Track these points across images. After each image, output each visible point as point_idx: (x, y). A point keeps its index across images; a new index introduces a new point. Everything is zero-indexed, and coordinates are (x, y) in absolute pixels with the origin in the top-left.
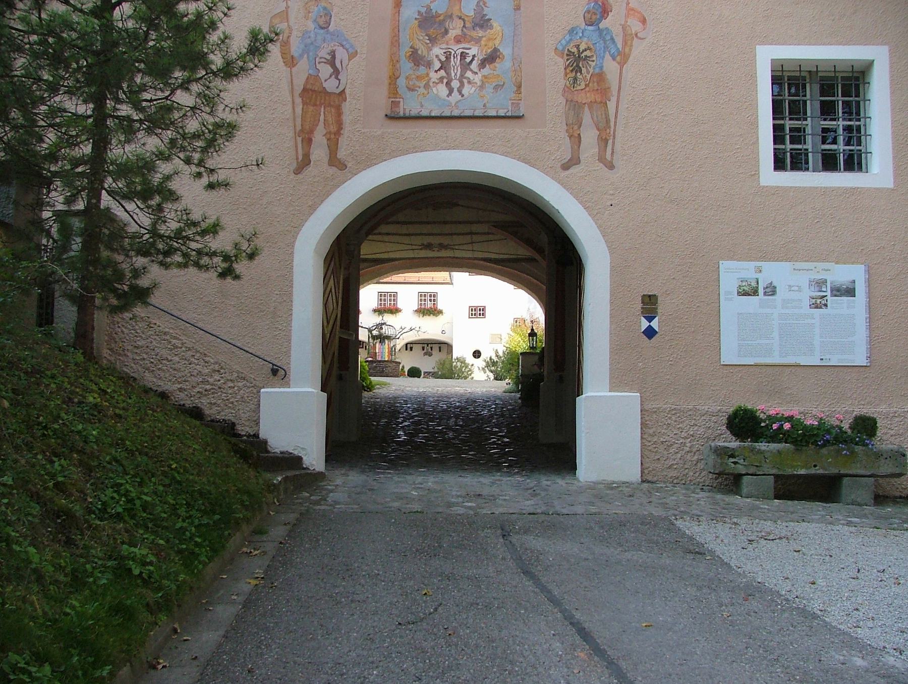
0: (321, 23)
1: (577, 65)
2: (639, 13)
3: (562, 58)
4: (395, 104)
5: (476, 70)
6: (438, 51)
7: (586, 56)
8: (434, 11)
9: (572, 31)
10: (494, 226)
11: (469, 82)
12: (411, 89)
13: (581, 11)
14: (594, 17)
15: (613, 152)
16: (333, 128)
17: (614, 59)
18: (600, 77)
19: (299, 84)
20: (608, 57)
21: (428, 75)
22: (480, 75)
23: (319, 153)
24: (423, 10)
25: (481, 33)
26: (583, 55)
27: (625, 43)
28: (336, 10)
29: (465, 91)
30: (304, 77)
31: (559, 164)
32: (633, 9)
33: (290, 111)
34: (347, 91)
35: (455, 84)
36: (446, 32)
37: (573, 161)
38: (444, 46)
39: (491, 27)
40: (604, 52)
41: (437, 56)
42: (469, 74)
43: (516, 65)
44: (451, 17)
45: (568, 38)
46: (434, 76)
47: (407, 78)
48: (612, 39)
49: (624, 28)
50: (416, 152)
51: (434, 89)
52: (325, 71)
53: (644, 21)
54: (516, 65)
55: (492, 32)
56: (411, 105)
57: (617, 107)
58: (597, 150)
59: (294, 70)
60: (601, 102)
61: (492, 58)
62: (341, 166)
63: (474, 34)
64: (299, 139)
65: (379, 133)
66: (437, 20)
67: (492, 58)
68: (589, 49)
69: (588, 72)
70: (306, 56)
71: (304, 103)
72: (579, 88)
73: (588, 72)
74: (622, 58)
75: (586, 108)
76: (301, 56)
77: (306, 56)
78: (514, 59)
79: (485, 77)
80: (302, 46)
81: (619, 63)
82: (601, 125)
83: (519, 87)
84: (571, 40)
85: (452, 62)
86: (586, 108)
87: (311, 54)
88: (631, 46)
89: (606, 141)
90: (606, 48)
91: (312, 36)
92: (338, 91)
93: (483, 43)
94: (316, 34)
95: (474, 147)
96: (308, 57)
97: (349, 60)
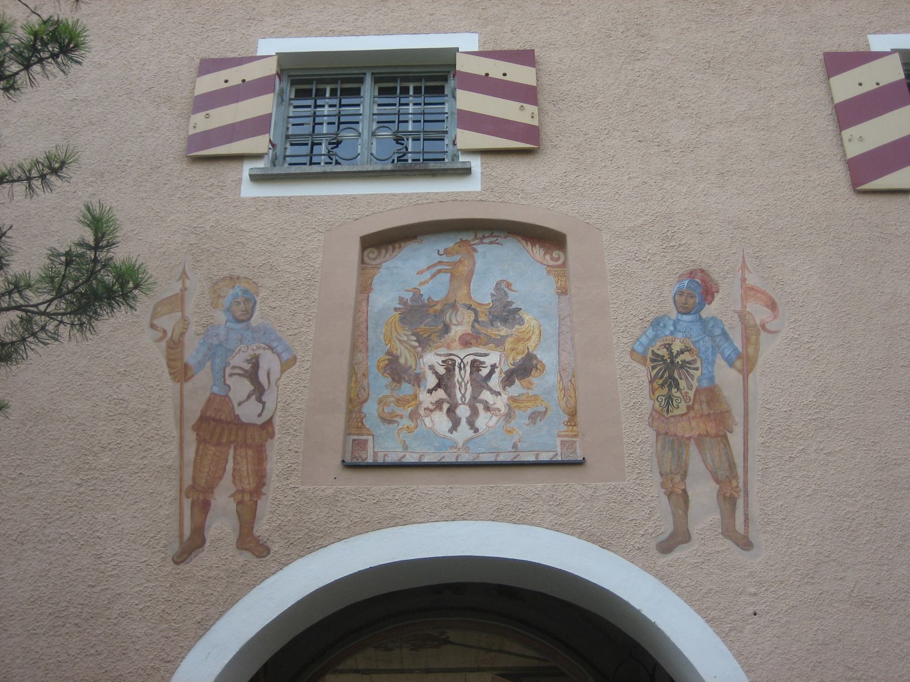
0: (238, 313)
1: (671, 376)
2: (764, 293)
3: (644, 364)
4: (360, 445)
6: (432, 359)
7: (684, 361)
8: (425, 297)
9: (657, 323)
10: (501, 675)
11: (487, 408)
12: (388, 420)
13: (669, 292)
14: (691, 301)
15: (747, 519)
16: (249, 484)
17: (731, 365)
18: (711, 394)
19: (195, 408)
20: (720, 361)
21: (415, 397)
22: (504, 397)
23: (222, 526)
24: (408, 296)
25: (504, 331)
26: (679, 359)
27: (746, 340)
28: (263, 293)
30: (203, 397)
31: (653, 544)
32: (752, 289)
33: (175, 453)
34: (277, 421)
35: (463, 412)
36: (447, 329)
37: (678, 538)
38: (443, 351)
39: (521, 322)
40: (714, 354)
41: (431, 367)
42: (486, 395)
43: (566, 380)
44: (454, 306)
45: (650, 333)
47: (380, 402)
48: (724, 334)
49: (742, 316)
50: (396, 525)
51: (427, 421)
52: (241, 388)
54: (566, 380)
55: (523, 328)
56: (386, 445)
57: (746, 443)
58: (718, 516)
59: (188, 386)
61: (525, 369)
62: (260, 550)
64: (187, 503)
65: (329, 492)
66: (431, 311)
67: (525, 369)
69: (690, 387)
70: (208, 364)
71: (200, 440)
72: (677, 412)
73: (690, 387)
74: (745, 363)
75: (693, 447)
76: (201, 365)
77: (208, 364)
78: (561, 371)
79: (513, 399)
81: (740, 371)
83: (573, 414)
84: (656, 337)
87: (218, 360)
88: (757, 343)
89: (732, 501)
90: (716, 349)
91: (222, 332)
92: (260, 421)
93: (508, 345)
95: (498, 515)
96: (213, 370)
97: (283, 371)
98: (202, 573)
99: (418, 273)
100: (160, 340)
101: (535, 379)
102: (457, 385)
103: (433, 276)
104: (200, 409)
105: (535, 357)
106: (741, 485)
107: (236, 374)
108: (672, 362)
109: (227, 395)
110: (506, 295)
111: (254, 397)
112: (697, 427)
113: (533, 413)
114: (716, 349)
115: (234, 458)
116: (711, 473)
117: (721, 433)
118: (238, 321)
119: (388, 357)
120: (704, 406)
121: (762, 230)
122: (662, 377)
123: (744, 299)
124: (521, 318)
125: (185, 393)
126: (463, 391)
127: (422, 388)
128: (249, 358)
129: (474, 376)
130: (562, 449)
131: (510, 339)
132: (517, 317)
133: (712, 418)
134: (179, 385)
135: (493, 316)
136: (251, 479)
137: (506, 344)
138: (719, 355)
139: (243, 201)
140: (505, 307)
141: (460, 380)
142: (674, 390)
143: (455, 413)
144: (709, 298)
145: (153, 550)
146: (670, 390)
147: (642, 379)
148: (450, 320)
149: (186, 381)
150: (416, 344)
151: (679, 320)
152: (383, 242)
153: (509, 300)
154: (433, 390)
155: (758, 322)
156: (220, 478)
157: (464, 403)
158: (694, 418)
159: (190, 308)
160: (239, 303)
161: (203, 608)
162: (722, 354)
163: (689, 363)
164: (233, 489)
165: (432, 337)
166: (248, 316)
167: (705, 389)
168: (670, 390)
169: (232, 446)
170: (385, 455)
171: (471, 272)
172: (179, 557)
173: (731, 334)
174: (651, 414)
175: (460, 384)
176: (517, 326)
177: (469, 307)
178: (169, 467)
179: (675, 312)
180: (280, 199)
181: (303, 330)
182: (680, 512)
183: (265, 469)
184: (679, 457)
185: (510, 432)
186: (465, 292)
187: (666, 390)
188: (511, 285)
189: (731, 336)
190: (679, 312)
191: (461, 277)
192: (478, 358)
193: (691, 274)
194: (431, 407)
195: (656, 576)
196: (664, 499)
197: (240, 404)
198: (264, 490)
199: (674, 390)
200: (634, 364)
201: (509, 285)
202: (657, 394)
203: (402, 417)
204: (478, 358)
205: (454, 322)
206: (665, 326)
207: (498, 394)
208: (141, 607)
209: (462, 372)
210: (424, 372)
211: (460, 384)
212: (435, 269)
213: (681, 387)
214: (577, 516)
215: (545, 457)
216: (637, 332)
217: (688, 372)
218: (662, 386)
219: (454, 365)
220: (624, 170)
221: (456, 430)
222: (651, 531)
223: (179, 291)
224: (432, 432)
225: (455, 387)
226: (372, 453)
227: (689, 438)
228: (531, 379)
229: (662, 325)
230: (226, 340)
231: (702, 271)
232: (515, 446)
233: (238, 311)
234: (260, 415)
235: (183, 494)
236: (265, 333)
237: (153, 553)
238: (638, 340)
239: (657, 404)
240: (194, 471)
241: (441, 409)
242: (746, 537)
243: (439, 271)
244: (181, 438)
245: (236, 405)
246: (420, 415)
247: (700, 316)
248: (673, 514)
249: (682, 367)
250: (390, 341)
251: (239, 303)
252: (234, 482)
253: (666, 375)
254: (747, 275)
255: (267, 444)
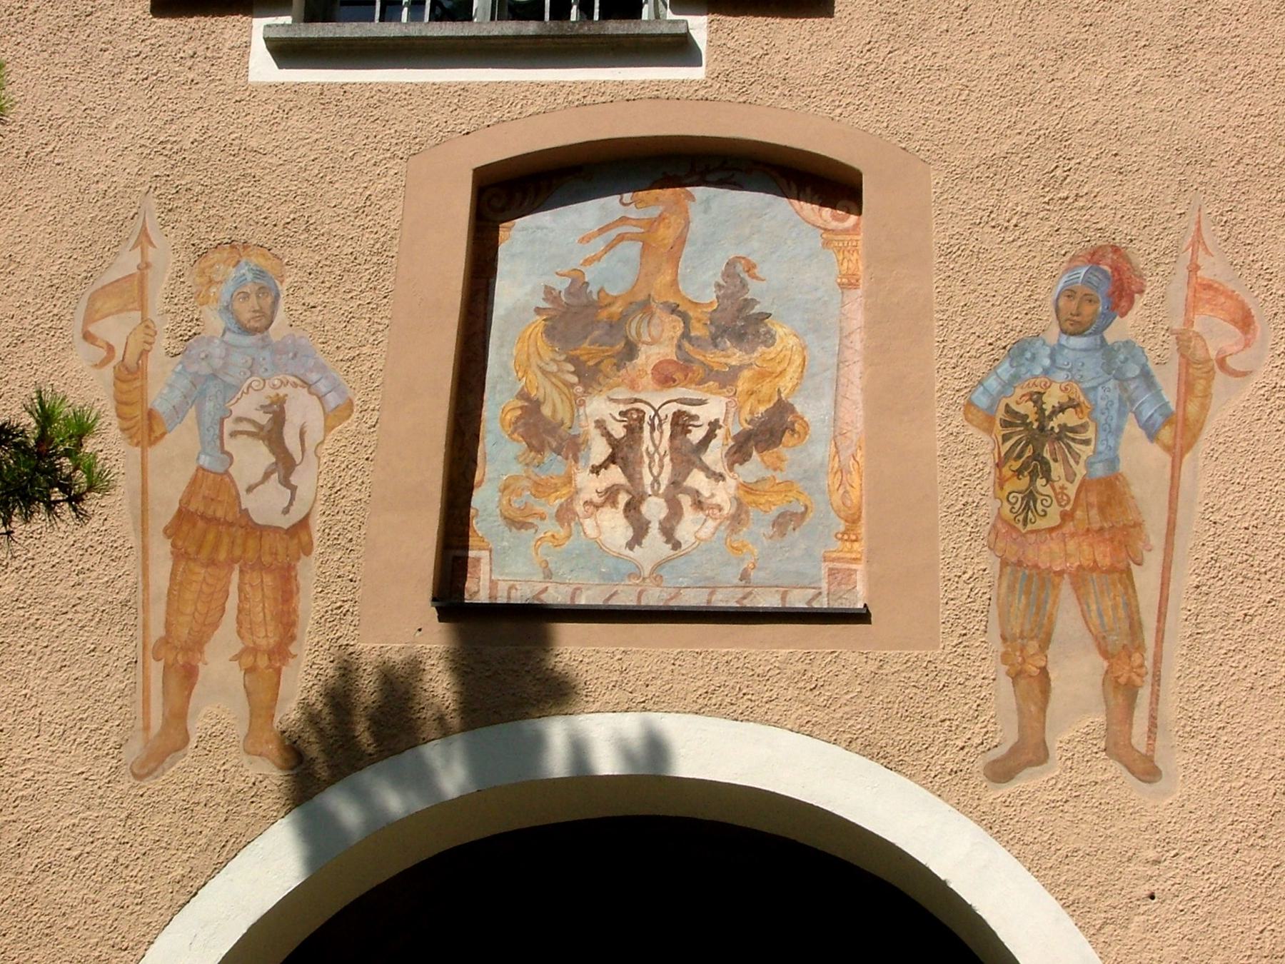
0: (246, 316)
1: (1037, 456)
2: (1230, 295)
3: (989, 431)
5: (720, 468)
6: (602, 407)
7: (1063, 427)
8: (593, 289)
9: (1019, 350)
11: (699, 504)
12: (517, 523)
13: (1048, 291)
14: (1088, 309)
15: (1153, 720)
16: (267, 637)
17: (1152, 436)
18: (1109, 491)
20: (1132, 428)
21: (569, 479)
22: (731, 482)
24: (562, 285)
25: (736, 357)
26: (1054, 424)
27: (1187, 387)
29: (687, 529)
31: (980, 763)
32: (1208, 287)
34: (317, 523)
35: (654, 509)
36: (631, 351)
37: (1026, 754)
38: (623, 393)
39: (769, 339)
40: (1122, 414)
41: (600, 424)
42: (697, 480)
45: (1005, 370)
46: (590, 485)
48: (1146, 375)
49: (1184, 341)
51: (588, 524)
52: (251, 459)
53: (1245, 321)
55: (772, 352)
58: (1101, 719)
59: (155, 453)
60: (1112, 570)
63: (713, 358)
64: (156, 669)
66: (603, 315)
68: (1073, 404)
69: (1070, 477)
70: (192, 412)
71: (179, 555)
72: (1042, 524)
73: (1070, 477)
74: (1179, 432)
75: (1066, 589)
76: (179, 412)
77: (192, 412)
79: (747, 488)
80: (185, 382)
81: (1168, 449)
82: (1116, 640)
84: (1016, 377)
85: (647, 443)
86: (1066, 589)
87: (209, 406)
88: (1207, 395)
89: (1130, 692)
90: (1127, 403)
91: (217, 350)
92: (286, 522)
93: (742, 385)
94: (229, 347)
97: (328, 429)
98: (183, 795)
99: (582, 240)
100: (103, 363)
101: (786, 450)
102: (646, 460)
103: (610, 247)
104: (179, 497)
105: (789, 408)
106: (1149, 664)
107: (242, 433)
108: (1042, 428)
109: (226, 472)
110: (744, 285)
111: (275, 476)
112: (1079, 552)
113: (782, 515)
114: (1127, 403)
115: (240, 590)
116: (1096, 638)
117: (1122, 566)
118: (246, 330)
119: (520, 403)
120: (1094, 512)
121: (1240, 168)
122: (1019, 456)
123: (1191, 306)
124: (768, 332)
125: (150, 466)
126: (656, 468)
127: (581, 463)
128: (267, 402)
129: (677, 442)
130: (830, 584)
131: (746, 373)
132: (762, 330)
133: (1107, 536)
134: (138, 450)
135: (717, 327)
136: (270, 628)
137: (740, 383)
138: (1131, 416)
139: (254, 91)
140: (740, 310)
141: (652, 449)
142: (1040, 482)
143: (639, 512)
144: (1124, 303)
145: (97, 753)
146: (1032, 481)
147: (982, 458)
148: (638, 334)
149: (153, 441)
150: (575, 379)
151: (1062, 346)
152: (509, 191)
153: (748, 296)
154: (601, 466)
155: (1213, 354)
156: (216, 625)
157: (656, 494)
158: (1073, 535)
159: (157, 302)
160: (246, 296)
161: (185, 857)
162: (1137, 415)
163: (1073, 430)
164: (238, 646)
165: (602, 366)
166: (264, 321)
167: (1099, 481)
168: (1032, 481)
169: (237, 567)
170: (510, 588)
171: (681, 240)
172: (143, 766)
173: (1159, 376)
174: (994, 526)
175: (651, 457)
176: (761, 349)
177: (674, 310)
178: (124, 604)
179: (1055, 329)
180: (323, 88)
181: (365, 350)
182: (1033, 708)
183: (295, 611)
184: (1039, 608)
185: (737, 549)
186: (668, 278)
187: (1025, 480)
188: (754, 266)
189: (1158, 379)
190: (1063, 331)
191: (664, 251)
192: (685, 408)
193: (1094, 256)
194: (597, 499)
195: (979, 822)
196: (1006, 684)
197: (250, 489)
198: (293, 649)
199: (1040, 482)
200: (971, 430)
201: (750, 267)
202: (1008, 487)
203: (543, 518)
204: (685, 408)
205: (646, 338)
206: (1034, 358)
207: (720, 477)
208: (75, 853)
209: (657, 434)
210: (587, 433)
211: (651, 457)
212: (613, 233)
213: (1054, 475)
214: (847, 709)
215: (798, 601)
216: (981, 367)
217: (1069, 447)
218: (1019, 473)
219: (641, 420)
220: (983, 38)
221: (640, 544)
222: (977, 741)
223: (135, 270)
224: (598, 547)
225: (641, 462)
226: (487, 583)
227: (1060, 574)
228: (781, 449)
229: (1028, 355)
230: (225, 365)
231: (1116, 249)
232: (744, 576)
233: (246, 311)
234: (286, 511)
235: (149, 653)
236: (295, 355)
237: (97, 758)
238: (980, 383)
239: (1007, 507)
240: (168, 613)
241: (614, 504)
242: (1149, 759)
243: (621, 238)
244: (145, 549)
245: (243, 493)
246: (576, 514)
247: (1103, 340)
248: (1020, 711)
249: (1059, 438)
250: (525, 372)
251: (246, 296)
252: (239, 633)
253: (1028, 453)
254: (1202, 259)
255: (299, 565)
